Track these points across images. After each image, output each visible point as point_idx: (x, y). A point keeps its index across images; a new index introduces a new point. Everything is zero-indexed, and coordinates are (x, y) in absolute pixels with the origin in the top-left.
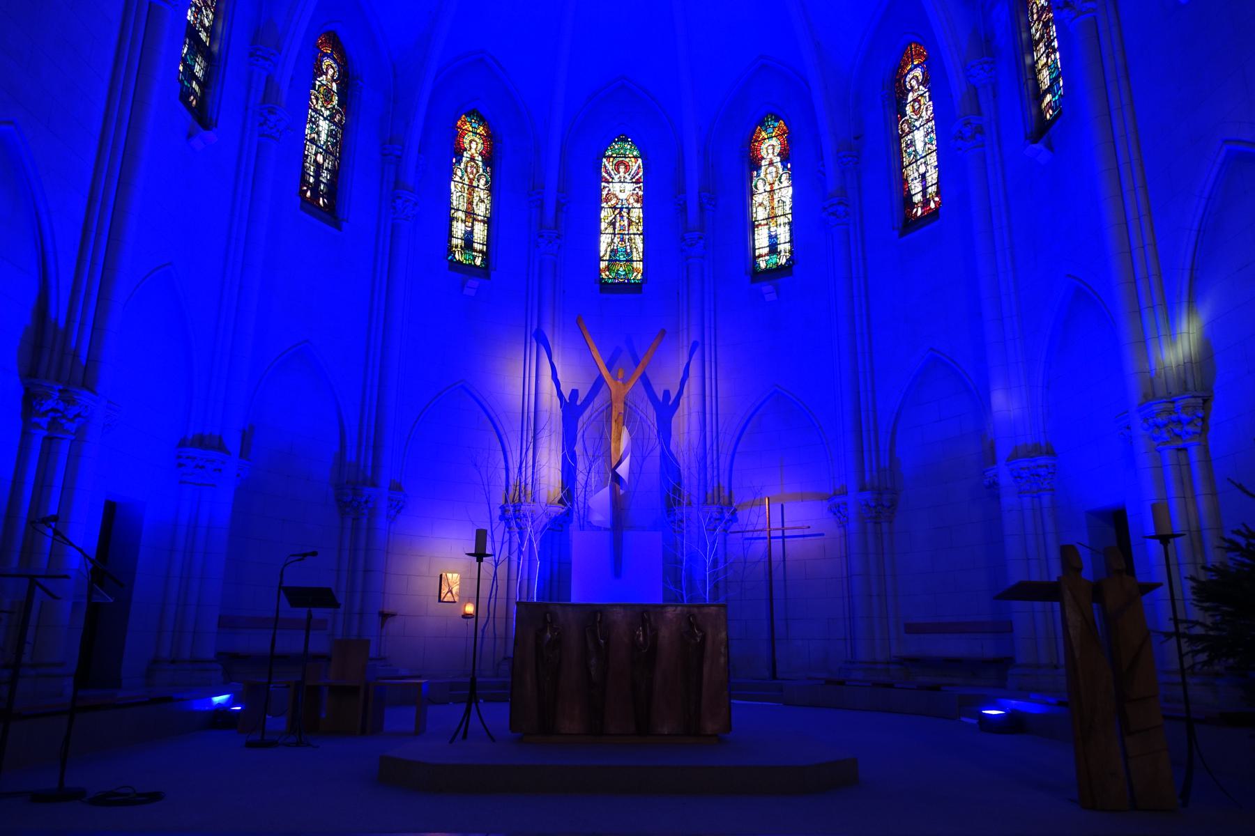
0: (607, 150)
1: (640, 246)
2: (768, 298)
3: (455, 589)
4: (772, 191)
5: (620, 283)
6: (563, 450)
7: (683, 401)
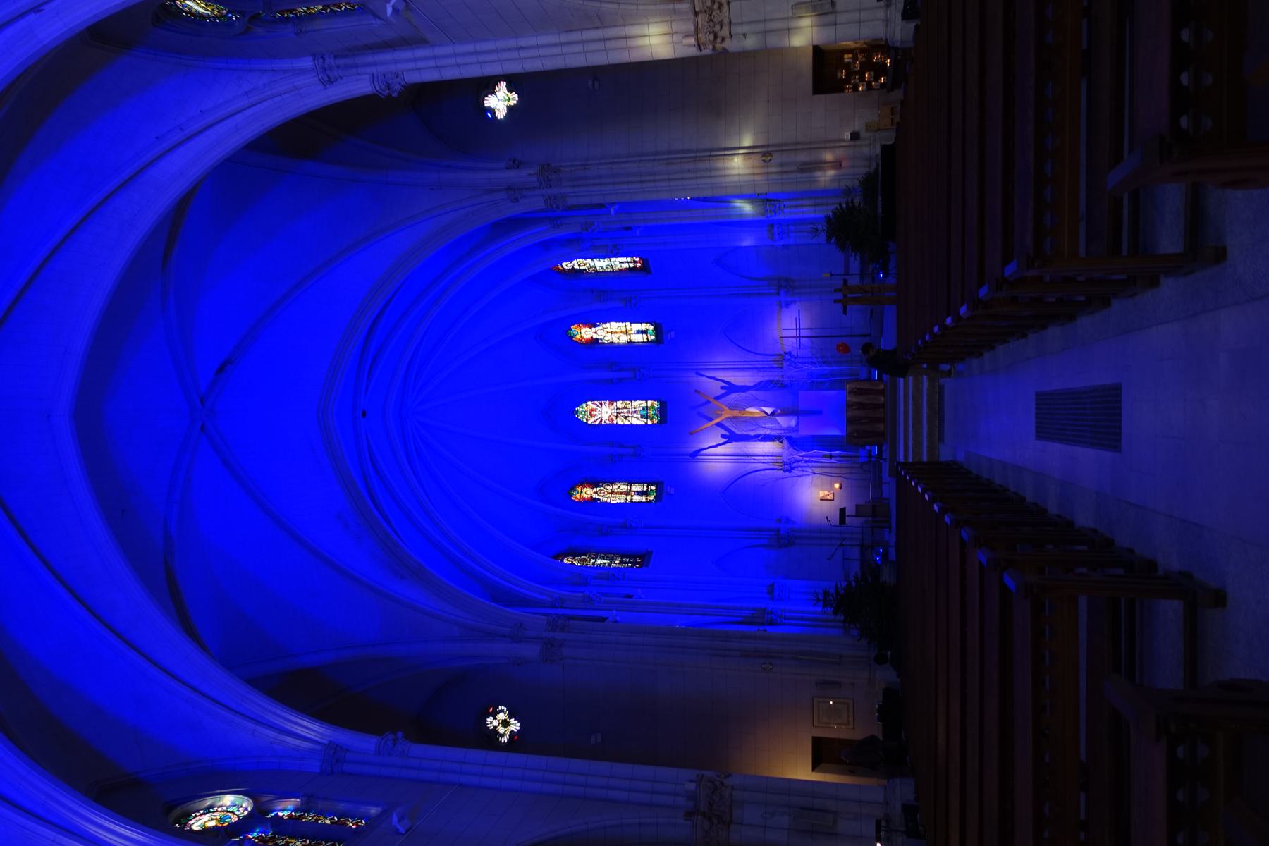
0: (583, 422)
1: (638, 402)
2: (673, 336)
3: (826, 493)
4: (612, 333)
5: (660, 413)
6: (756, 441)
7: (727, 379)
